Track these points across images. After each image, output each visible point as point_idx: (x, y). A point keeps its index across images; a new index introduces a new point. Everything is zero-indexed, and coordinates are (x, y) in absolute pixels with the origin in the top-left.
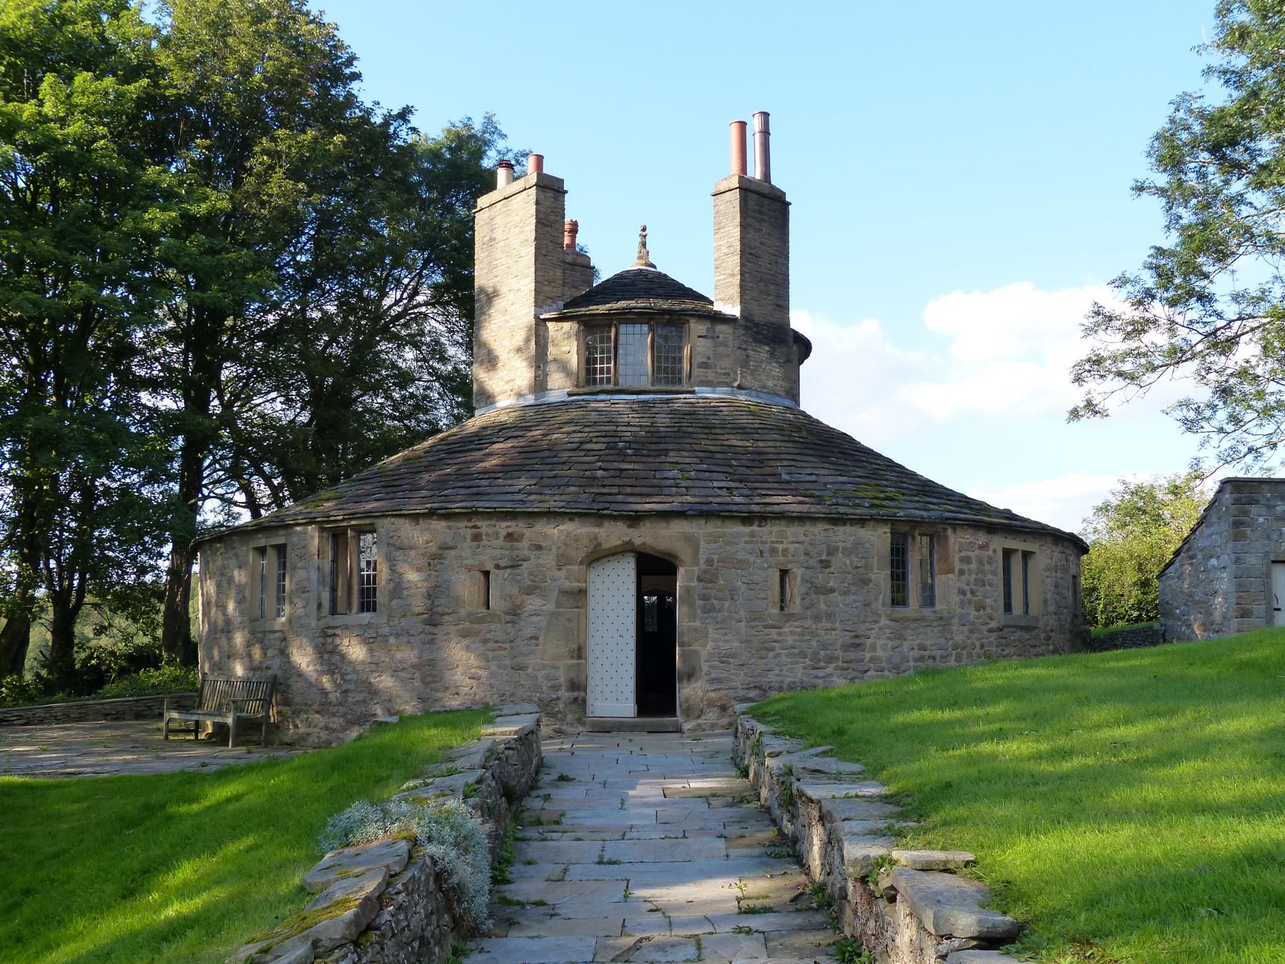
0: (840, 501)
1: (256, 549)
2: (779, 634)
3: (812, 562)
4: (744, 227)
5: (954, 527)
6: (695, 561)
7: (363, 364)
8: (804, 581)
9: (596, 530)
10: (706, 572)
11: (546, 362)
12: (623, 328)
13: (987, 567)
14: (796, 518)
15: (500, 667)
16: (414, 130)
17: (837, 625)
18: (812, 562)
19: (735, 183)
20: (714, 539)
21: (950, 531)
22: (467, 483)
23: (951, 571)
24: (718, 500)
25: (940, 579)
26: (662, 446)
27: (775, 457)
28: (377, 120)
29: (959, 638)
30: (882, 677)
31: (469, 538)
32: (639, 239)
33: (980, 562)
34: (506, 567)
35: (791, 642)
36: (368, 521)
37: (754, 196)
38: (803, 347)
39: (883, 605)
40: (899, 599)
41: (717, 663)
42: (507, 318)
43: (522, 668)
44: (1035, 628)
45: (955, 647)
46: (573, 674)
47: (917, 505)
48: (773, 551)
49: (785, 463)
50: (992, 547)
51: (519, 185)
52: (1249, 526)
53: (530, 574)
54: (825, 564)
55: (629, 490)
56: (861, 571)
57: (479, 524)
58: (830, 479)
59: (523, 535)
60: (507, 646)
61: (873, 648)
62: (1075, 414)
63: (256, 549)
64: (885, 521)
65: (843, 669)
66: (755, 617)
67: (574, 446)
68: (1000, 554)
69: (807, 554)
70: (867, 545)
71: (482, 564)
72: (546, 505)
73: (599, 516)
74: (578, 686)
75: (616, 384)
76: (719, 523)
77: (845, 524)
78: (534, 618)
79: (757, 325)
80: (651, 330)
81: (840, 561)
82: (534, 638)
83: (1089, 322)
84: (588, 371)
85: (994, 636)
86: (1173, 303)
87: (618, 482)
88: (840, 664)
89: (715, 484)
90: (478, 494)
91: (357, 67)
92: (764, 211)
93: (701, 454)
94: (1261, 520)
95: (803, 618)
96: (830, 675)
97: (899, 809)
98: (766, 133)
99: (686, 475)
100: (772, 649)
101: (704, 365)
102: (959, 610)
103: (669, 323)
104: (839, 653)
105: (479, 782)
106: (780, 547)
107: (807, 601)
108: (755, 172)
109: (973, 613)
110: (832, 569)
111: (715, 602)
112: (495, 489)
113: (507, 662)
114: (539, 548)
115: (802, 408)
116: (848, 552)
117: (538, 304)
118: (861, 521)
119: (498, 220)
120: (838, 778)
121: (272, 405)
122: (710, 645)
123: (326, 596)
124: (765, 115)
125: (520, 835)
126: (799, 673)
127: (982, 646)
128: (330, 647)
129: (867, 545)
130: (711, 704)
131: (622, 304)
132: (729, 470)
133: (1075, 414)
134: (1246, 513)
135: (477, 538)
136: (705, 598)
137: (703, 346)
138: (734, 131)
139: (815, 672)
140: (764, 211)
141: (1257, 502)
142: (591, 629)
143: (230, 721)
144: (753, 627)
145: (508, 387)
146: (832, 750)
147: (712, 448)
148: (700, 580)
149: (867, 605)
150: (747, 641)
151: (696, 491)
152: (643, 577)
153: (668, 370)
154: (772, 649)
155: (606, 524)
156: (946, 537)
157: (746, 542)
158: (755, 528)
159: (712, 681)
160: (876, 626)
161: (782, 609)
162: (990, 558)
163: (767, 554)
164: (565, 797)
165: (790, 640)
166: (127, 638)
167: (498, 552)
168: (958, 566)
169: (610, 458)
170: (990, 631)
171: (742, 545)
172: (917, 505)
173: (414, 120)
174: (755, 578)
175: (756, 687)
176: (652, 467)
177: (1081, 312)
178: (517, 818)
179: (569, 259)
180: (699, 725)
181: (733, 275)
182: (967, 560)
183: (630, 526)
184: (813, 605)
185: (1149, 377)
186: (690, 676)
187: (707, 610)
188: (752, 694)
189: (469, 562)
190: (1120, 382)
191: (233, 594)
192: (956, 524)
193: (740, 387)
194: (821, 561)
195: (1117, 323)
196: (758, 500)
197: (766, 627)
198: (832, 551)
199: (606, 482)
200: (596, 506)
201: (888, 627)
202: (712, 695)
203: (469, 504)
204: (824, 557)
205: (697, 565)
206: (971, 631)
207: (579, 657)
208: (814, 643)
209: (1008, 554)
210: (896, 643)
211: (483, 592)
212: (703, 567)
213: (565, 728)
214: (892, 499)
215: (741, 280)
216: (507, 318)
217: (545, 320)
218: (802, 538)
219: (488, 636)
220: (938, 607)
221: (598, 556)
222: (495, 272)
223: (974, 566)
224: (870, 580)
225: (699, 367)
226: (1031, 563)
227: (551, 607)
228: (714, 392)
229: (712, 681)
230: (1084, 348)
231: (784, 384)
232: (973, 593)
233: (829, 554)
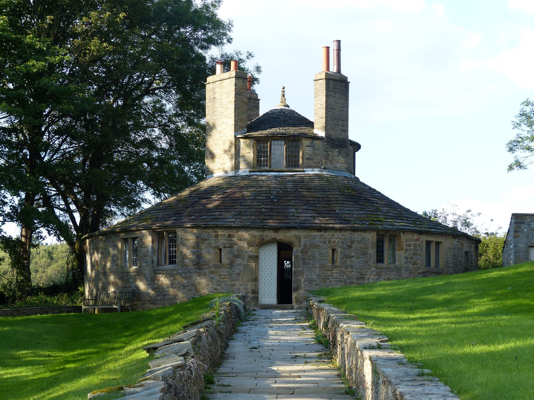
0: (357, 222)
2: (331, 273)
3: (345, 246)
4: (327, 96)
5: (404, 233)
6: (300, 245)
8: (341, 253)
9: (262, 233)
10: (304, 249)
11: (239, 157)
12: (273, 142)
13: (418, 248)
15: (225, 285)
18: (345, 246)
19: (323, 76)
20: (306, 237)
21: (402, 234)
23: (402, 249)
24: (309, 222)
25: (397, 253)
26: (289, 198)
32: (281, 93)
33: (415, 246)
36: (173, 229)
38: (357, 147)
39: (373, 263)
40: (380, 259)
42: (222, 135)
46: (253, 288)
48: (330, 242)
49: (339, 205)
51: (227, 75)
52: (520, 232)
54: (350, 247)
56: (364, 249)
57: (218, 231)
58: (356, 212)
60: (228, 277)
61: (369, 279)
62: (511, 168)
64: (374, 231)
66: (322, 267)
68: (424, 243)
69: (343, 243)
70: (367, 240)
71: (219, 246)
72: (243, 224)
74: (255, 292)
75: (270, 167)
76: (309, 231)
77: (358, 231)
78: (239, 267)
79: (333, 140)
80: (286, 143)
81: (356, 245)
84: (258, 161)
87: (270, 214)
92: (337, 87)
93: (305, 202)
94: (525, 230)
95: (340, 267)
98: (339, 50)
100: (329, 279)
103: (293, 140)
104: (355, 281)
106: (332, 240)
107: (342, 261)
108: (333, 69)
109: (411, 266)
112: (222, 217)
116: (359, 242)
117: (236, 131)
118: (364, 230)
119: (217, 89)
123: (155, 258)
124: (339, 42)
131: (273, 130)
133: (511, 168)
134: (519, 227)
136: (303, 259)
137: (308, 150)
138: (324, 51)
140: (337, 87)
141: (524, 223)
142: (269, 246)
144: (321, 270)
145: (222, 167)
148: (301, 252)
149: (366, 262)
150: (320, 276)
152: (282, 251)
153: (292, 162)
154: (329, 279)
155: (266, 231)
156: (400, 236)
157: (319, 238)
158: (323, 233)
161: (333, 264)
162: (420, 244)
163: (327, 243)
165: (336, 275)
168: (405, 247)
169: (268, 203)
171: (317, 239)
174: (322, 252)
176: (284, 207)
181: (322, 118)
182: (409, 245)
183: (275, 232)
184: (344, 262)
186: (297, 289)
187: (304, 264)
189: (213, 245)
191: (110, 258)
193: (324, 168)
194: (348, 246)
197: (326, 270)
198: (353, 242)
200: (262, 224)
201: (374, 271)
206: (410, 273)
207: (256, 282)
208: (345, 277)
209: (428, 243)
210: (377, 277)
211: (219, 256)
212: (302, 247)
214: (379, 221)
215: (326, 120)
216: (222, 135)
217: (239, 138)
218: (341, 237)
220: (397, 263)
221: (263, 243)
222: (216, 113)
224: (367, 253)
225: (306, 160)
226: (440, 246)
228: (313, 171)
230: (512, 135)
231: (345, 165)
232: (411, 258)
233: (351, 243)
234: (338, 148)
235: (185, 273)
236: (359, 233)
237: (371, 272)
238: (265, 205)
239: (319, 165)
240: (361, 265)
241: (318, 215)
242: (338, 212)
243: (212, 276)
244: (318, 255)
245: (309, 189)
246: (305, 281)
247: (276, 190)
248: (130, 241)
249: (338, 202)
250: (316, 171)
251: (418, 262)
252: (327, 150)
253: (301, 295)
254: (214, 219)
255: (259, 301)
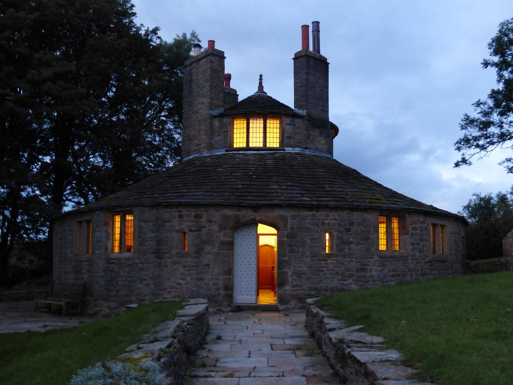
0: (355, 200)
1: (78, 222)
2: (326, 264)
3: (342, 229)
5: (409, 214)
7: (136, 143)
8: (338, 238)
9: (238, 213)
14: (333, 208)
16: (159, 37)
17: (353, 260)
20: (294, 218)
21: (407, 215)
22: (177, 191)
23: (408, 234)
24: (297, 199)
26: (270, 174)
27: (323, 179)
28: (142, 32)
29: (412, 266)
30: (375, 285)
31: (177, 216)
33: (421, 230)
34: (195, 231)
35: (331, 268)
36: (129, 209)
37: (313, 60)
38: (334, 130)
41: (296, 278)
42: (198, 115)
43: (202, 279)
44: (446, 261)
45: (409, 271)
47: (391, 202)
48: (323, 224)
49: (328, 182)
50: (427, 222)
53: (206, 234)
54: (348, 230)
55: (253, 194)
57: (182, 210)
58: (350, 190)
59: (203, 215)
60: (195, 268)
61: (371, 270)
62: (457, 165)
63: (78, 222)
65: (357, 281)
67: (228, 174)
69: (339, 225)
72: (214, 201)
73: (239, 206)
74: (229, 288)
82: (208, 265)
83: (463, 123)
85: (427, 266)
86: (502, 114)
88: (355, 278)
89: (295, 192)
90: (182, 196)
91: (135, 10)
93: (288, 178)
96: (350, 284)
97: (415, 371)
99: (281, 187)
100: (323, 271)
101: (289, 138)
102: (411, 253)
105: (169, 346)
106: (327, 222)
109: (418, 254)
110: (351, 233)
111: (295, 248)
113: (195, 276)
114: (210, 221)
115: (334, 158)
120: (371, 346)
121: (97, 160)
122: (293, 268)
124: (316, 24)
125: (193, 373)
126: (335, 283)
127: (422, 270)
128: (111, 269)
129: (368, 221)
130: (293, 297)
132: (301, 185)
133: (457, 165)
135: (181, 217)
136: (290, 246)
139: (343, 282)
140: (312, 68)
142: (235, 261)
143: (63, 304)
144: (313, 260)
146: (364, 328)
147: (294, 175)
148: (288, 237)
149: (368, 250)
150: (311, 267)
151: (286, 195)
154: (323, 271)
155: (243, 211)
157: (310, 219)
158: (314, 213)
159: (294, 286)
160: (372, 260)
163: (320, 225)
164: (221, 348)
165: (331, 266)
166: (31, 261)
167: (191, 224)
168: (411, 231)
169: (245, 179)
170: (426, 263)
171: (308, 221)
172: (391, 202)
173: (159, 33)
174: (315, 237)
175: (315, 289)
177: (459, 119)
178: (192, 364)
179: (227, 91)
180: (287, 308)
182: (415, 229)
183: (254, 211)
185: (491, 148)
187: (292, 251)
188: (313, 293)
189: (177, 228)
190: (478, 150)
192: (410, 212)
194: (346, 229)
195: (475, 123)
196: (315, 199)
197: (319, 260)
198: (351, 224)
199: (243, 190)
200: (238, 201)
202: (294, 293)
203: (177, 200)
204: (347, 227)
205: (287, 230)
206: (417, 263)
208: (343, 268)
213: (222, 308)
216: (198, 115)
218: (337, 217)
219: (186, 264)
223: (418, 231)
224: (369, 238)
225: (287, 138)
227: (216, 250)
228: (294, 150)
229: (294, 286)
230: (461, 134)
231: (326, 147)
232: (418, 244)
234: (319, 128)
235: (142, 263)
236: (359, 213)
237: (374, 261)
238: (241, 181)
239: (300, 145)
240: (363, 253)
241: (306, 192)
242: (328, 189)
243: (175, 267)
244: (309, 241)
245: (292, 166)
246: (293, 273)
247: (254, 166)
248: (84, 224)
249: (326, 179)
250: (297, 150)
251: (425, 248)
252: (308, 129)
253: (288, 292)
254: (179, 196)
255: (234, 299)
